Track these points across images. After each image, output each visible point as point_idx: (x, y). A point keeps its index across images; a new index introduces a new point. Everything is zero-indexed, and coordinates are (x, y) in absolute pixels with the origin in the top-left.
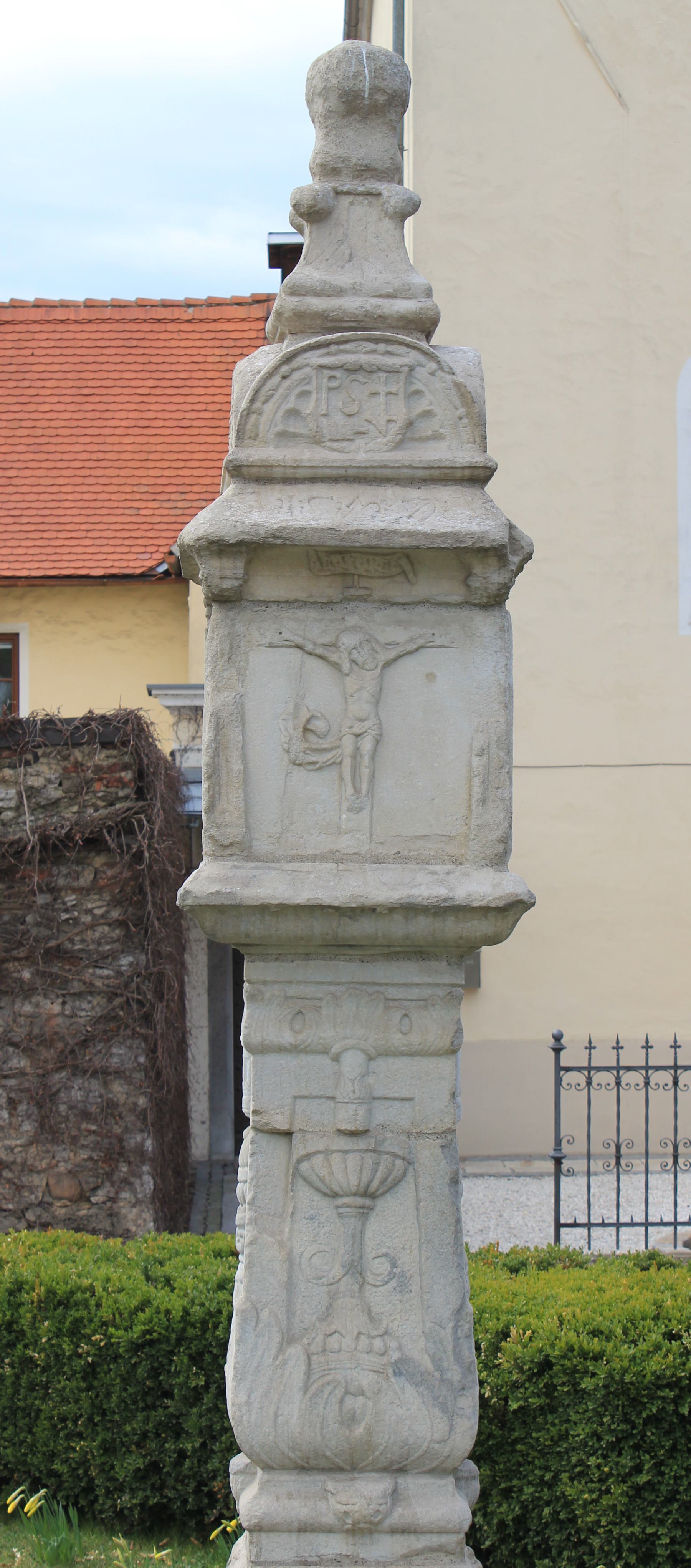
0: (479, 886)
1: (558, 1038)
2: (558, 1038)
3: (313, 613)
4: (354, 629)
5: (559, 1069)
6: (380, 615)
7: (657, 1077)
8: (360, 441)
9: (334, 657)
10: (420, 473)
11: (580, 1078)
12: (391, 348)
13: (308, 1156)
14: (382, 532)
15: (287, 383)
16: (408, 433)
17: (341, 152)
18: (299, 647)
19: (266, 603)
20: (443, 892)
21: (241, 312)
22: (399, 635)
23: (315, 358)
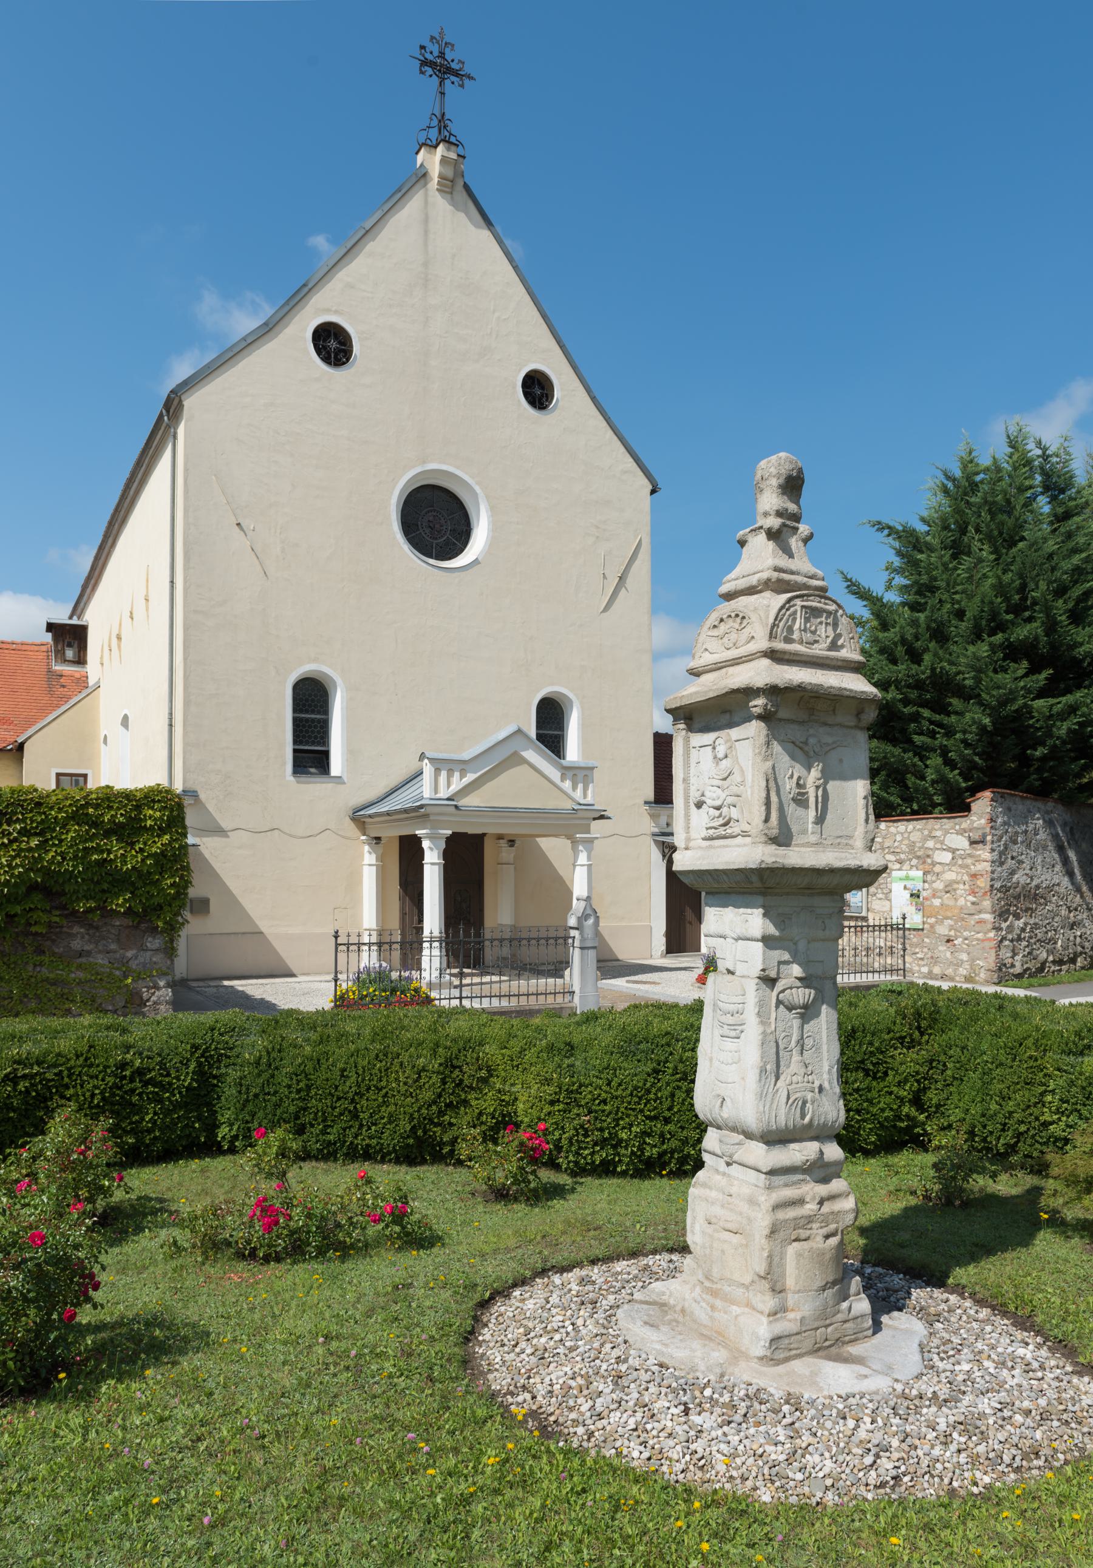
0: (870, 861)
1: (337, 932)
2: (337, 932)
5: (337, 945)
6: (821, 730)
7: (352, 947)
8: (816, 645)
9: (806, 749)
10: (840, 663)
11: (344, 948)
13: (783, 991)
14: (840, 689)
16: (834, 646)
17: (785, 506)
18: (793, 743)
19: (780, 720)
20: (858, 863)
21: (36, 648)
22: (830, 740)
23: (799, 602)
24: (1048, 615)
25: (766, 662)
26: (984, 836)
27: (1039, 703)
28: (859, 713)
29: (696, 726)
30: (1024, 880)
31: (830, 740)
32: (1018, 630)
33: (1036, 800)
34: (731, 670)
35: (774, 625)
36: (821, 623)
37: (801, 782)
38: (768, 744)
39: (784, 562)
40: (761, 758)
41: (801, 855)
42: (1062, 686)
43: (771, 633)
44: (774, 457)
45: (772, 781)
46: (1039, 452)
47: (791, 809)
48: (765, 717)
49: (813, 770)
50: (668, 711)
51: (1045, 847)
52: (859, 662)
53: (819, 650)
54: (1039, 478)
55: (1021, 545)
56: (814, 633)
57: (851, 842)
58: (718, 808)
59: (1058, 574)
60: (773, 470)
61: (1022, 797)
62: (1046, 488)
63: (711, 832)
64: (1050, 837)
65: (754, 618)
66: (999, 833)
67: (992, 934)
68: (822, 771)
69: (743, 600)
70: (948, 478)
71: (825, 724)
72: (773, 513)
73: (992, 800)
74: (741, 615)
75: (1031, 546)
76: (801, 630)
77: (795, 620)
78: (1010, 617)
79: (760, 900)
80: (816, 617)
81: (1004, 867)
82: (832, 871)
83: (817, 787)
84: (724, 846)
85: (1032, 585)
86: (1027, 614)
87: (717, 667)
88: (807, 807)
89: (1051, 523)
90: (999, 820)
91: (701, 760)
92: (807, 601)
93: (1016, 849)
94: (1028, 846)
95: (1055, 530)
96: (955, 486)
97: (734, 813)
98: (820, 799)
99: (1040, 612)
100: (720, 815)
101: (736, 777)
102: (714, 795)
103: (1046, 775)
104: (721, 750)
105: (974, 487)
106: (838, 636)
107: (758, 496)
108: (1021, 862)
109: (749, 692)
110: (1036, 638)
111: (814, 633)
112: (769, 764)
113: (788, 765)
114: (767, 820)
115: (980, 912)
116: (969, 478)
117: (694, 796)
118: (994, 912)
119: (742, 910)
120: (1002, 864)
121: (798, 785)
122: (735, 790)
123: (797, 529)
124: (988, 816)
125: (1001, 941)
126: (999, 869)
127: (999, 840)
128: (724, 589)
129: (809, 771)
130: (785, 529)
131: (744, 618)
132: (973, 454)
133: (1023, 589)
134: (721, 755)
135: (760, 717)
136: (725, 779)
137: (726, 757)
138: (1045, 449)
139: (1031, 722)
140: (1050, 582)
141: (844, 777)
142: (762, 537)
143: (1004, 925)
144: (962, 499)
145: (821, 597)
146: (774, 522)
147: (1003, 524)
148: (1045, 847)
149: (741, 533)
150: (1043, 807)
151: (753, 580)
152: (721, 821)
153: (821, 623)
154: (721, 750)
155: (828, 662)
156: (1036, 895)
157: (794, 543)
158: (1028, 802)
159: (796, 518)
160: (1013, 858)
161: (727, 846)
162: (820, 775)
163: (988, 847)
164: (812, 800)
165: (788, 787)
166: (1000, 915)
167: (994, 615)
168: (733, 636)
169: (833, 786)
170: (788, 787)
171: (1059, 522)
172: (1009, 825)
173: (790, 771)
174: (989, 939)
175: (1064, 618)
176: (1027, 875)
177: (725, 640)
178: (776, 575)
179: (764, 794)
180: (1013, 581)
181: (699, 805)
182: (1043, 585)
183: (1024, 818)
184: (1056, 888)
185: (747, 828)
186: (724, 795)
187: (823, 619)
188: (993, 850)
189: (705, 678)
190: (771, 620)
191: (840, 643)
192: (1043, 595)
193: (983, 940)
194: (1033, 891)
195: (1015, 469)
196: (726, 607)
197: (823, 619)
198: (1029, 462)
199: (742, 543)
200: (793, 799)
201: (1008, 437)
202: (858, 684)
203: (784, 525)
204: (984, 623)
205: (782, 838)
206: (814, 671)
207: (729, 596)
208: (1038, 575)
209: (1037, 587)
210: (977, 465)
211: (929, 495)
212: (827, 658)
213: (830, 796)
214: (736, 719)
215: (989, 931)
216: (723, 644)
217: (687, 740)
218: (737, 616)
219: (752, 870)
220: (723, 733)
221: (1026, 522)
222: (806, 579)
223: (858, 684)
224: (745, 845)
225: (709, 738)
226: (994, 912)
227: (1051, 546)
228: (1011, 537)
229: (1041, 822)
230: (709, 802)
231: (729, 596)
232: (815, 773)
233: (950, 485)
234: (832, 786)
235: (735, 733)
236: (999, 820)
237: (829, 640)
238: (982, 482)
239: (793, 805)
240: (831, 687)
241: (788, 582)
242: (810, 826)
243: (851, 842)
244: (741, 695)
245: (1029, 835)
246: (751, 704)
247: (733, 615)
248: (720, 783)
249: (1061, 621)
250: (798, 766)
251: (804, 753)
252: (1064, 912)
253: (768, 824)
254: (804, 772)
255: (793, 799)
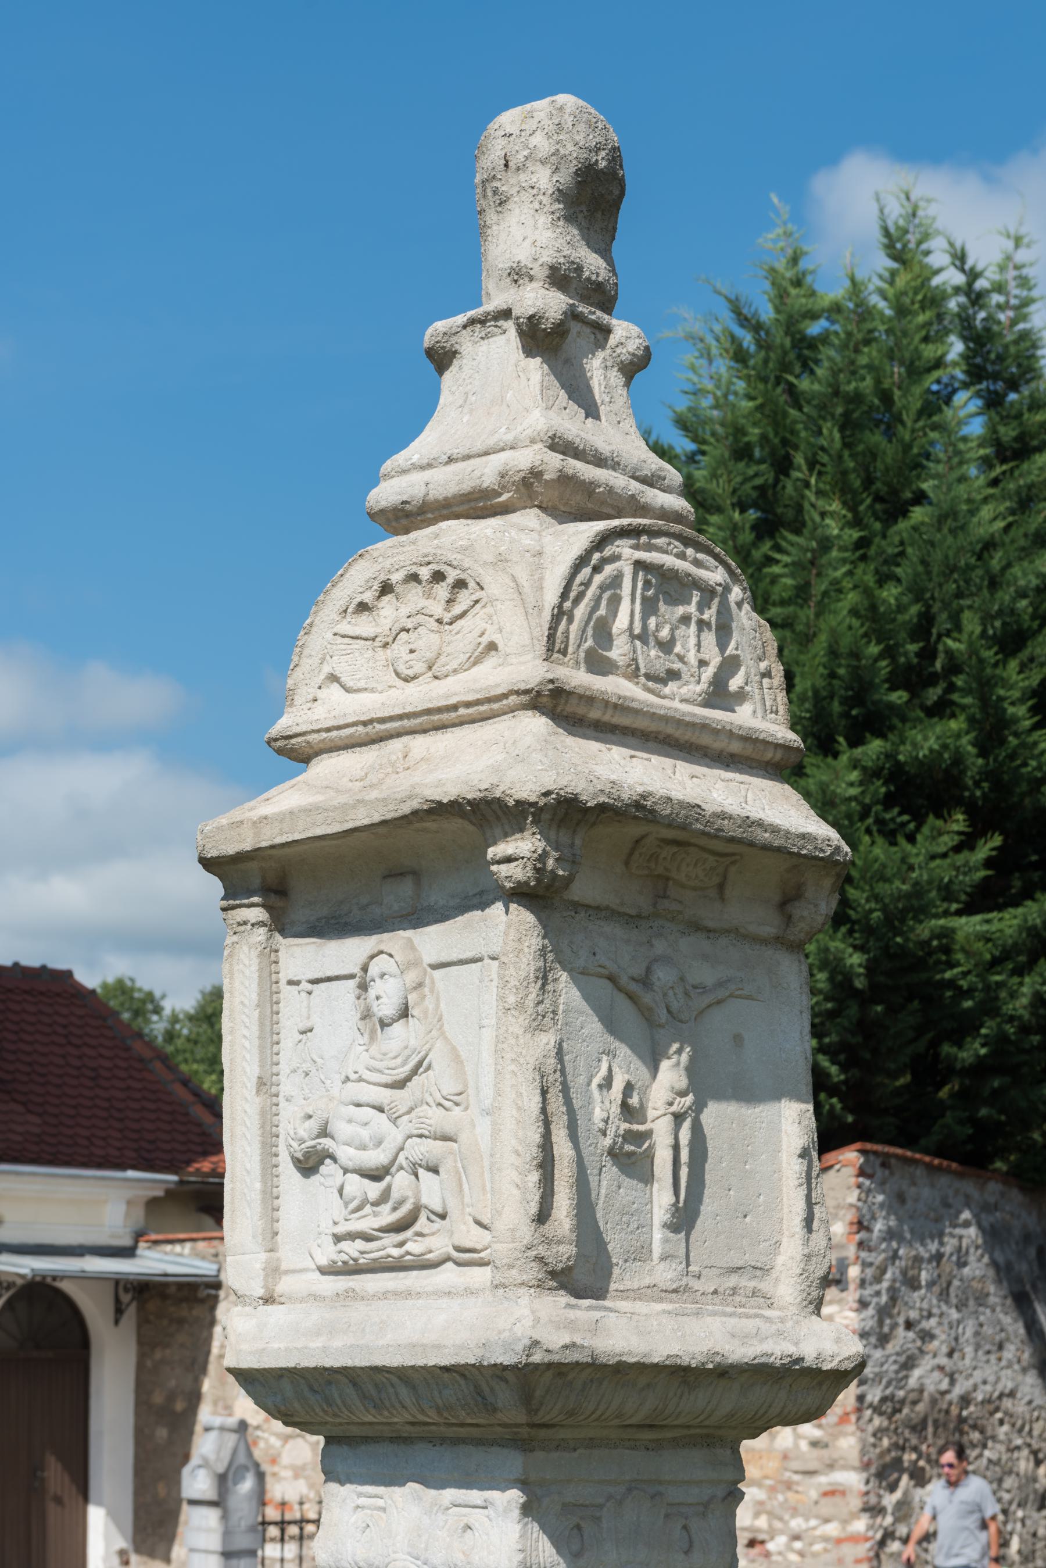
3: (615, 929)
4: (665, 960)
8: (671, 687)
9: (647, 999)
10: (735, 747)
12: (700, 556)
14: (747, 822)
15: (598, 579)
16: (719, 694)
17: (574, 255)
18: (612, 979)
19: (577, 906)
20: (791, 1349)
22: (705, 974)
23: (625, 548)
24: (984, 701)
25: (535, 725)
26: (843, 1265)
27: (969, 926)
28: (787, 901)
29: (300, 914)
30: (935, 1383)
31: (705, 974)
32: (915, 734)
33: (960, 1175)
34: (419, 744)
35: (560, 614)
36: (685, 619)
37: (634, 1101)
38: (544, 978)
39: (572, 424)
40: (523, 1020)
41: (637, 1327)
42: (1017, 884)
43: (551, 637)
44: (541, 106)
45: (557, 1090)
46: (960, 279)
47: (607, 1179)
48: (536, 896)
49: (665, 1065)
50: (209, 864)
51: (981, 1299)
52: (786, 748)
53: (682, 700)
54: (956, 348)
55: (918, 514)
56: (666, 647)
57: (764, 1286)
58: (375, 1175)
59: (1005, 596)
60: (541, 143)
61: (929, 1167)
62: (976, 373)
63: (353, 1248)
64: (991, 1273)
65: (496, 585)
66: (877, 1258)
67: (860, 1525)
68: (691, 1070)
69: (450, 537)
70: (744, 320)
71: (696, 927)
72: (540, 272)
73: (862, 1173)
74: (452, 575)
75: (941, 519)
76: (633, 637)
77: (615, 602)
78: (898, 697)
79: (514, 1462)
80: (674, 601)
81: (891, 1348)
82: (724, 1373)
83: (678, 1118)
84: (396, 1294)
85: (943, 621)
86: (933, 694)
87: (373, 733)
88: (647, 1177)
89: (987, 463)
90: (879, 1226)
91: (316, 1021)
92: (649, 548)
93: (918, 1300)
94: (944, 1295)
95: (995, 482)
96: (759, 343)
97: (431, 1191)
98: (684, 1155)
99: (966, 691)
100: (384, 1197)
101: (440, 1079)
102: (365, 1134)
103: (983, 1112)
104: (387, 995)
105: (805, 351)
106: (730, 665)
107: (491, 217)
108: (927, 1336)
109: (492, 813)
110: (958, 760)
111: (666, 647)
112: (548, 1040)
113: (594, 1048)
114: (542, 1216)
115: (831, 1466)
116: (791, 323)
117: (295, 1131)
118: (866, 1466)
119: (450, 1494)
120: (883, 1340)
121: (628, 1111)
122: (435, 1118)
123: (607, 331)
124: (851, 1215)
125: (882, 1543)
126: (878, 1354)
127: (878, 1279)
128: (386, 493)
129: (654, 1070)
130: (575, 327)
131: (460, 584)
132: (803, 264)
133: (923, 627)
134: (387, 1008)
135: (521, 895)
136: (400, 1084)
137: (404, 1013)
138: (973, 275)
139: (948, 975)
140: (986, 618)
141: (747, 1092)
142: (506, 342)
143: (890, 1500)
144: (778, 381)
145: (687, 542)
146: (552, 304)
147: (874, 456)
148: (981, 1299)
149: (441, 325)
150: (975, 1194)
151: (485, 473)
152: (387, 1216)
153: (685, 619)
154: (387, 995)
155: (706, 740)
156: (962, 1420)
157: (599, 372)
158: (944, 1180)
159: (603, 296)
160: (909, 1325)
161: (408, 1294)
162: (683, 1083)
163: (852, 1295)
164: (663, 1157)
165: (598, 1114)
166: (880, 1475)
167: (860, 690)
168: (427, 640)
169: (717, 1115)
170: (598, 1114)
171: (1004, 461)
172: (901, 1239)
173: (609, 1068)
174: (854, 1539)
175: (1021, 711)
176: (941, 1368)
177: (399, 649)
178: (554, 461)
179: (535, 1136)
180: (901, 608)
181: (309, 1164)
182: (971, 623)
183: (934, 1223)
184: (1007, 1403)
185: (474, 1237)
186: (394, 1136)
187: (692, 609)
188: (863, 1304)
189: (324, 767)
190: (551, 597)
191: (735, 684)
192: (973, 652)
193: (839, 1541)
194: (954, 1411)
195: (902, 311)
196: (394, 554)
197: (692, 609)
198: (934, 300)
199: (441, 359)
200: (611, 1152)
201: (887, 233)
202: (782, 811)
203: (572, 315)
204: (836, 707)
205: (582, 1275)
206: (668, 762)
207: (404, 518)
208: (959, 595)
209: (958, 627)
210: (813, 294)
211: (690, 356)
212: (704, 727)
213: (710, 1145)
214: (435, 897)
215: (854, 1516)
216: (392, 663)
217: (270, 957)
218: (438, 577)
219: (500, 1371)
220: (394, 941)
221: (928, 456)
222: (635, 486)
223: (782, 811)
224: (470, 1292)
225: (346, 953)
226: (866, 1466)
227: (988, 520)
228: (895, 492)
229: (972, 1231)
230: (347, 1154)
231: (404, 518)
232: (671, 1075)
233: (747, 339)
234: (713, 1114)
235: (433, 941)
236: (879, 1226)
237: (708, 673)
238: (824, 339)
239: (611, 1171)
240: (724, 816)
241: (588, 488)
242: (658, 1235)
243: (936, 1289)
244: (456, 824)
245: (947, 1266)
246: (494, 852)
247: (425, 573)
248: (384, 1096)
249: (1015, 720)
250: (623, 1051)
251: (644, 1017)
252: (1024, 1465)
253: (548, 1228)
254: (640, 1071)
255: (611, 1152)
